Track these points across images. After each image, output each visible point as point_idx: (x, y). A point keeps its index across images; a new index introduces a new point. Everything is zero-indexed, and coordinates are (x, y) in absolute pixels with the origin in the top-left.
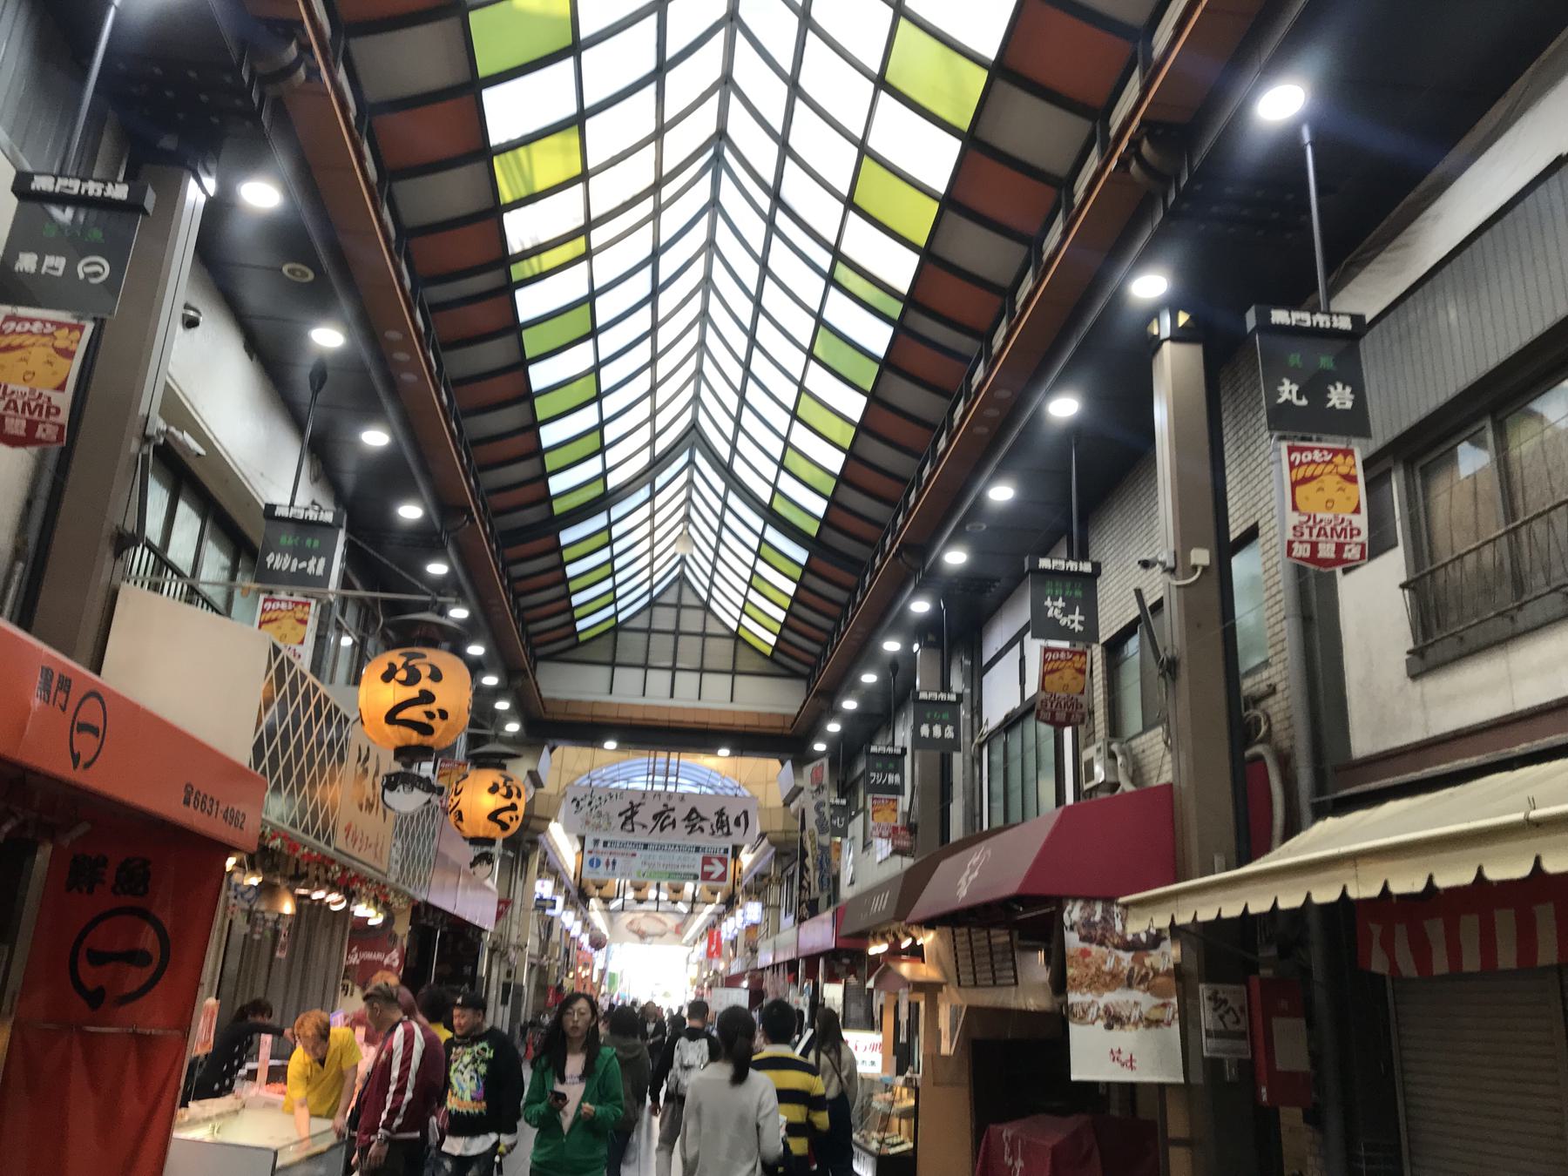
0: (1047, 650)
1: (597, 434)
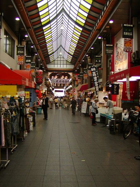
0: (125, 40)
1: (47, 4)
